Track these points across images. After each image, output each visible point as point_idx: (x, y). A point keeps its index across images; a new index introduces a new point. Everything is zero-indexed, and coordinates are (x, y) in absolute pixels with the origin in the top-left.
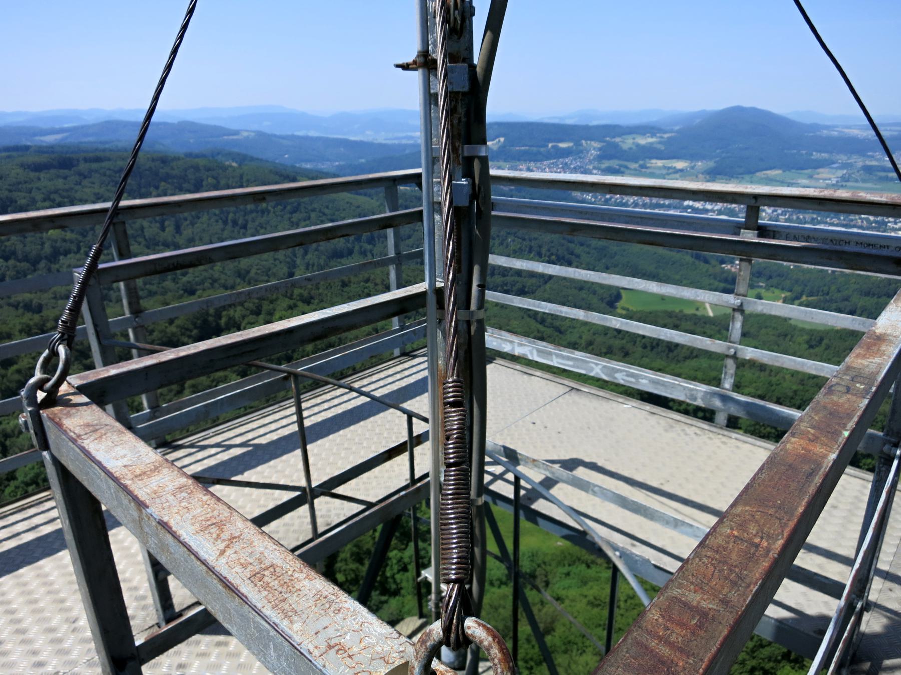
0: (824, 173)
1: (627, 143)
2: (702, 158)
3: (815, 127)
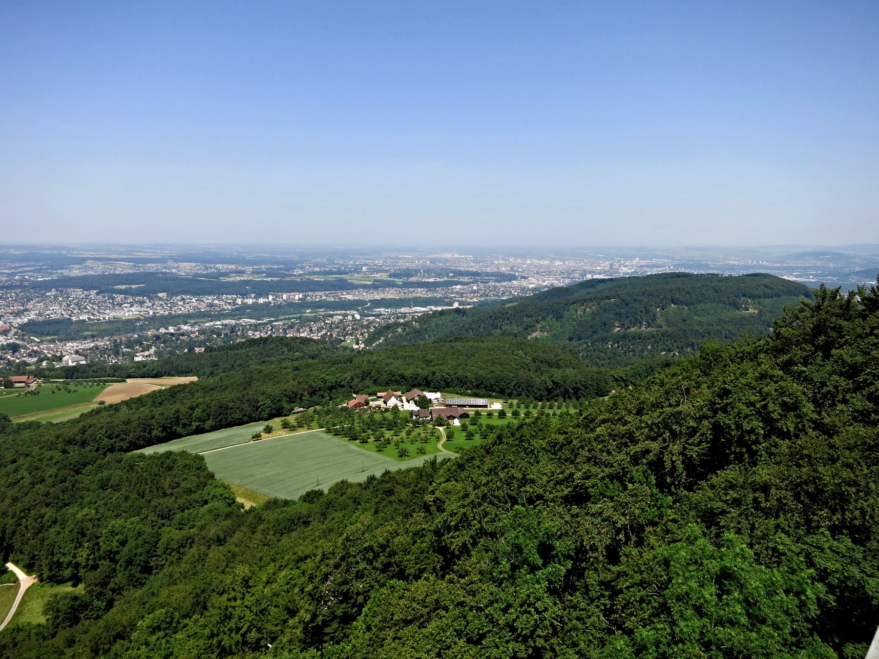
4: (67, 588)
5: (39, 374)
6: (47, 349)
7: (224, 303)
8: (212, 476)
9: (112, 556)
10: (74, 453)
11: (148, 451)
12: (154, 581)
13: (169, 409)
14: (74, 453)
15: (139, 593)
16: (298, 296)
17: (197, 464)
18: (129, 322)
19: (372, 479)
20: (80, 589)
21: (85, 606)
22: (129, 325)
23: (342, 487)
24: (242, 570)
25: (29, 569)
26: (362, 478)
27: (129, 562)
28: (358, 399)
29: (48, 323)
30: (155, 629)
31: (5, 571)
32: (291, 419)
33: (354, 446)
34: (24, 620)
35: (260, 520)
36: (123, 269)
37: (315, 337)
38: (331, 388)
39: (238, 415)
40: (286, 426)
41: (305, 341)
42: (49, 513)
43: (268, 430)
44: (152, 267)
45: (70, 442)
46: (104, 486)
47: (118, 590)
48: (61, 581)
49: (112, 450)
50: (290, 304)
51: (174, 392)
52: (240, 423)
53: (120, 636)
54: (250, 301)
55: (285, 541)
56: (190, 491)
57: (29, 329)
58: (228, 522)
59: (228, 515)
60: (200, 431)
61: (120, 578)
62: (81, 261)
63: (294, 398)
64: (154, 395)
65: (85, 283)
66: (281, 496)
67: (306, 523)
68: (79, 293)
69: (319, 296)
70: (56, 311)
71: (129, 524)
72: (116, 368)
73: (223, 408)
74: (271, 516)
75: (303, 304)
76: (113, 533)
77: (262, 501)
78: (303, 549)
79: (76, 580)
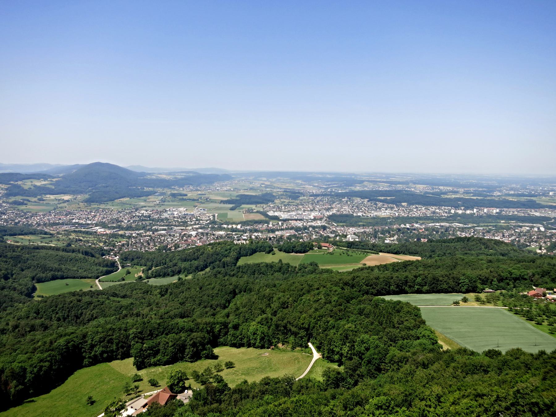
0: (152, 198)
1: (27, 185)
2: (81, 192)
3: (143, 174)
4: (335, 366)
5: (335, 243)
6: (340, 230)
7: (442, 211)
8: (424, 322)
9: (360, 355)
10: (347, 291)
11: (387, 298)
12: (382, 378)
13: (402, 275)
14: (347, 291)
15: (372, 382)
16: (495, 211)
17: (415, 313)
18: (384, 219)
19: (542, 353)
20: (342, 369)
21: (343, 379)
22: (383, 221)
23: (516, 353)
24: (437, 389)
25: (319, 349)
26: (535, 351)
27: (369, 362)
28: (536, 290)
29: (342, 216)
30: (379, 407)
31: (307, 347)
32: (482, 296)
33: (530, 325)
34: (313, 376)
35: (453, 360)
36: (384, 187)
37: (506, 240)
38: (516, 279)
39: (445, 286)
40: (478, 300)
41: (497, 242)
42: (332, 321)
43: (465, 300)
44: (400, 187)
45: (346, 284)
46: (361, 312)
47: (361, 376)
48: (333, 361)
49: (367, 293)
50: (489, 216)
51: (406, 265)
52: (446, 292)
53: (358, 403)
54: (460, 212)
55: (469, 379)
56: (409, 329)
57: (332, 218)
58: (431, 355)
59: (432, 351)
60: (419, 292)
61: (363, 369)
62: (361, 182)
63: (485, 281)
64: (394, 265)
65: (362, 195)
66: (470, 347)
67: (486, 372)
68: (358, 200)
69: (512, 212)
70: (346, 210)
71: (373, 339)
72: (374, 246)
73: (435, 280)
74: (461, 359)
75: (499, 217)
76: (362, 342)
77: (456, 348)
78: (481, 389)
79: (340, 364)
